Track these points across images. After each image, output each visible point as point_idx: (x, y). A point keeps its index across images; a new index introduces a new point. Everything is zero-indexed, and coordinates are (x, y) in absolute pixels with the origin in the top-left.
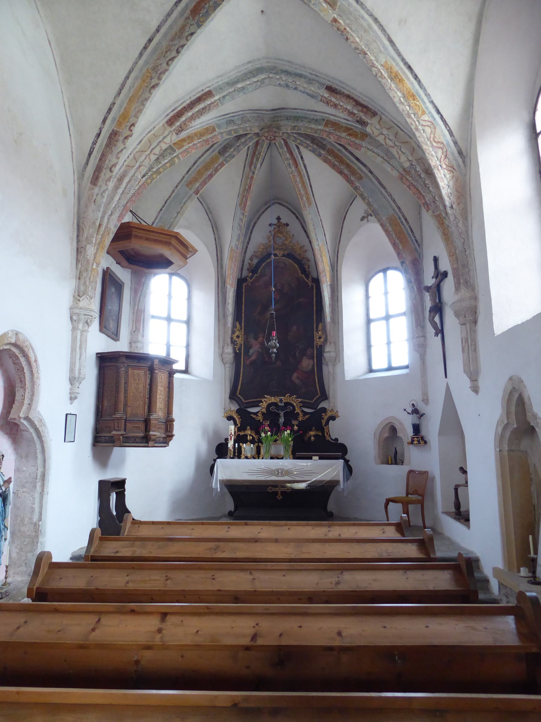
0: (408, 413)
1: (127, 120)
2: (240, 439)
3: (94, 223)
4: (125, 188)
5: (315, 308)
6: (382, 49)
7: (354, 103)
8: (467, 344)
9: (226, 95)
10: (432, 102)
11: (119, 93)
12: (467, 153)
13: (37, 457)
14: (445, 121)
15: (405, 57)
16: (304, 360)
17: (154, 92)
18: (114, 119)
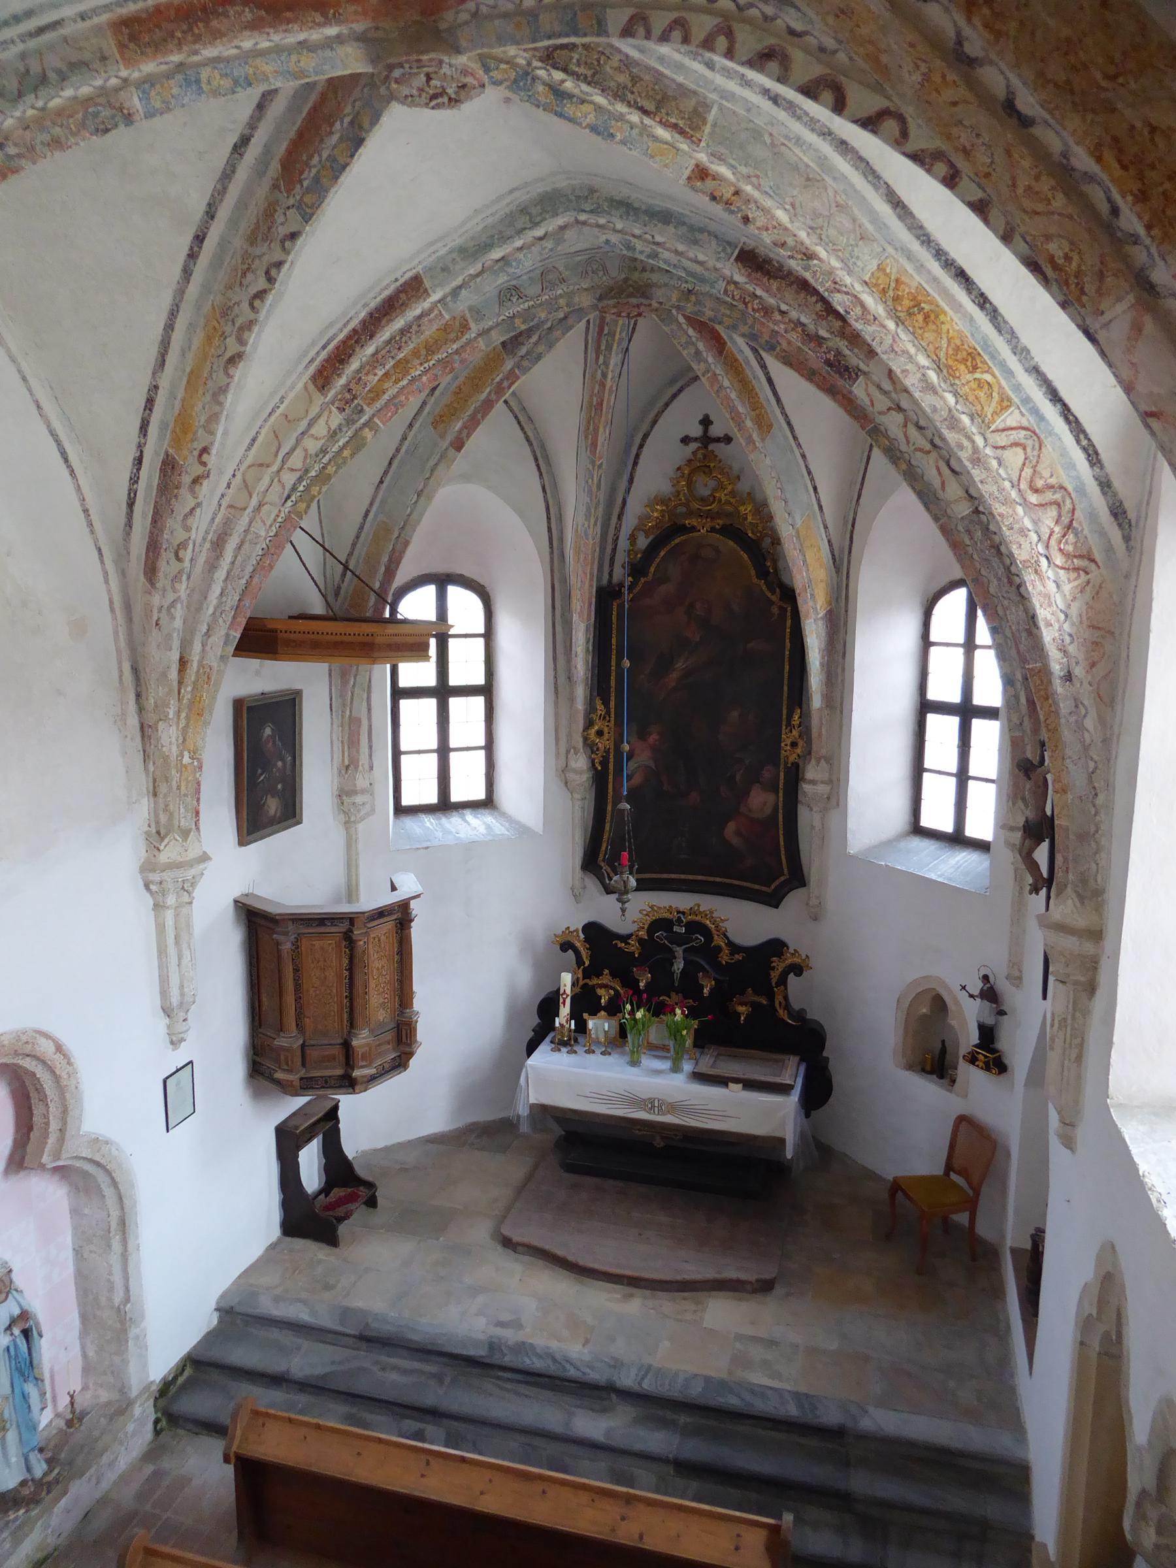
0: (971, 996)
1: (190, 436)
2: (585, 1003)
3: (164, 674)
4: (233, 563)
5: (787, 668)
6: (870, 227)
7: (819, 306)
8: (1061, 1034)
9: (460, 287)
10: (1036, 371)
11: (161, 363)
12: (1138, 518)
13: (104, 1196)
14: (1077, 421)
15: (945, 245)
16: (752, 793)
17: (237, 372)
18: (164, 426)
